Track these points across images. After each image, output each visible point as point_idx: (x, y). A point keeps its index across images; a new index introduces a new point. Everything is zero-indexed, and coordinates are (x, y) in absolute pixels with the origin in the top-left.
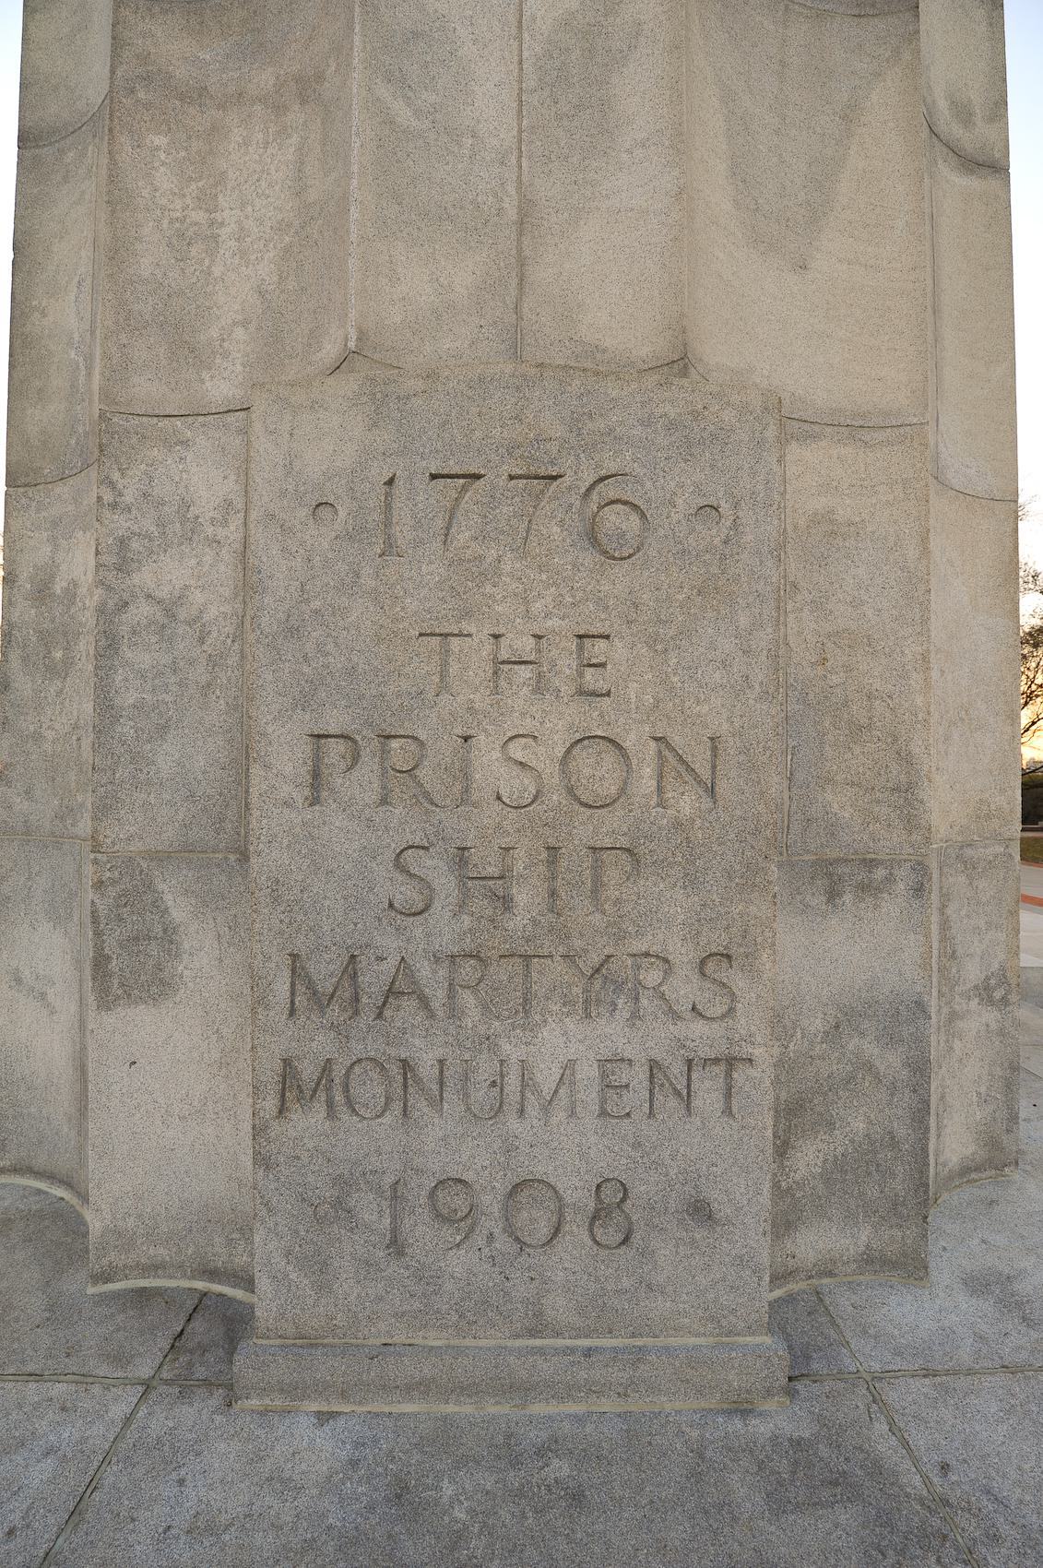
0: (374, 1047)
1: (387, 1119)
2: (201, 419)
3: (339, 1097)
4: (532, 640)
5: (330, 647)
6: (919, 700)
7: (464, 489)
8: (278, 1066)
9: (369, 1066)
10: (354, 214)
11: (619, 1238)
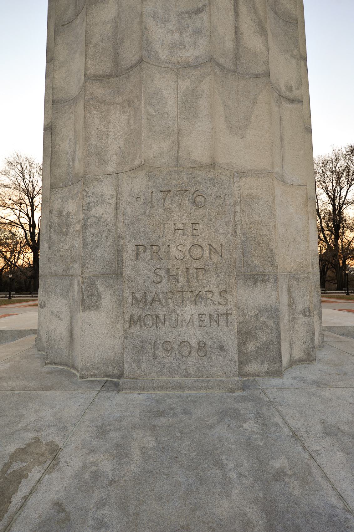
0: (150, 312)
1: (153, 328)
2: (106, 176)
3: (142, 323)
4: (182, 225)
5: (140, 227)
6: (274, 236)
7: (167, 194)
8: (129, 316)
9: (149, 316)
10: (143, 135)
11: (204, 354)
